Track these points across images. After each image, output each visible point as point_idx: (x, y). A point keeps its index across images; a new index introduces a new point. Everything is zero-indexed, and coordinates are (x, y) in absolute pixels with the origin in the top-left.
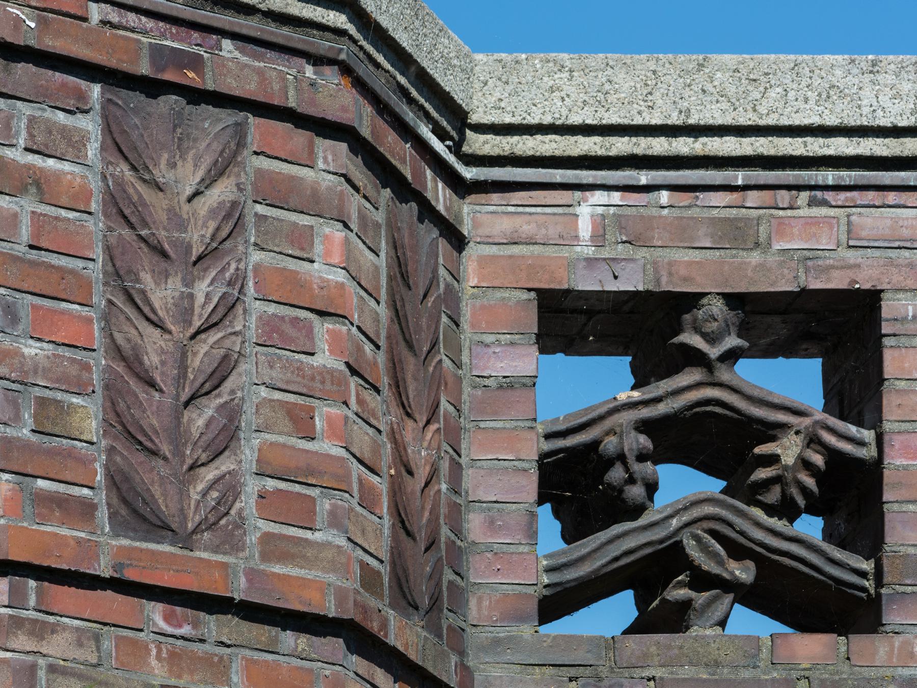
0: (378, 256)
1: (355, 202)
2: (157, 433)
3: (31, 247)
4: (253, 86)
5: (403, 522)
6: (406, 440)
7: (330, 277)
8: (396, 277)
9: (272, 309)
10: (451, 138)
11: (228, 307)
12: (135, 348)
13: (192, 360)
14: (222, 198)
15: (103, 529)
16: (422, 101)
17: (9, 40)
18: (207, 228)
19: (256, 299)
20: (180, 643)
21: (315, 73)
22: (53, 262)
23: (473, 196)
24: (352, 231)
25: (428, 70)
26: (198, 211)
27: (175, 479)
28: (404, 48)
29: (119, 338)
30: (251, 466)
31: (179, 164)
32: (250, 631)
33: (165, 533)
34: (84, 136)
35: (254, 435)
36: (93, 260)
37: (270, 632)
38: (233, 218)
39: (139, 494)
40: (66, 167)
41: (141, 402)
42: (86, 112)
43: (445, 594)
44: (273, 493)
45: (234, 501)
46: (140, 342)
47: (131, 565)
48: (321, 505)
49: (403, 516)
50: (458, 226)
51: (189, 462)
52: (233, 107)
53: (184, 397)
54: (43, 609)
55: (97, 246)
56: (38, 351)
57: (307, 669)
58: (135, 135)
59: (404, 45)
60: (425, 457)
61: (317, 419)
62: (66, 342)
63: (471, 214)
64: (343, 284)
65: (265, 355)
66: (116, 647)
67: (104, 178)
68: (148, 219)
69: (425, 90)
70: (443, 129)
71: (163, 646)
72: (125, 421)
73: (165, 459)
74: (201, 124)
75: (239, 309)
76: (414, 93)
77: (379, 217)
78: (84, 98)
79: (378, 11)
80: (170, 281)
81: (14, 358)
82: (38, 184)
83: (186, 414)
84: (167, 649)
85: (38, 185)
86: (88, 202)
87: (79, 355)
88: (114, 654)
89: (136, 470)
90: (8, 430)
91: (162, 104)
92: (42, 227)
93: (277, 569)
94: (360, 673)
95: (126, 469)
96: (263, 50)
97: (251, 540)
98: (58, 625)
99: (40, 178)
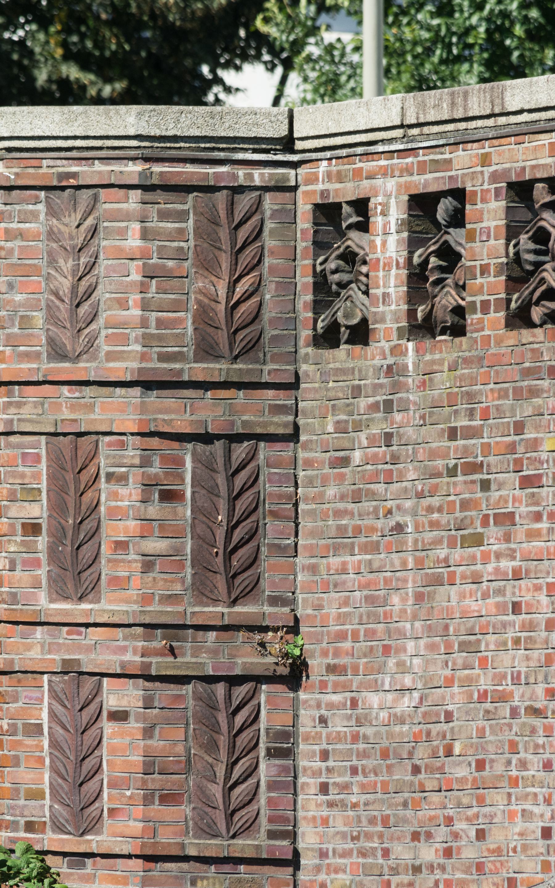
40: (33, 225)
82: (21, 234)
83: (79, 310)
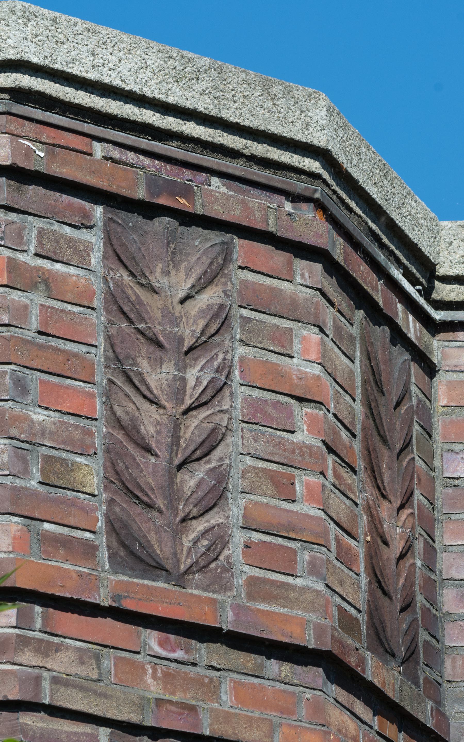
0: (353, 363)
1: (329, 315)
2: (152, 489)
3: (40, 333)
4: (237, 213)
5: (379, 582)
6: (381, 515)
7: (308, 370)
8: (369, 382)
9: (256, 393)
10: (421, 284)
11: (215, 391)
12: (133, 419)
13: (185, 433)
14: (211, 301)
15: (103, 566)
16: (393, 247)
17: (21, 165)
18: (197, 324)
19: (241, 385)
20: (173, 665)
21: (293, 208)
22: (59, 346)
23: (442, 334)
24: (328, 336)
25: (397, 222)
26: (189, 312)
27: (169, 528)
28: (374, 199)
29: (119, 411)
30: (238, 520)
31: (173, 272)
32: (238, 658)
33: (159, 572)
34: (88, 246)
35: (240, 495)
36: (96, 346)
37: (256, 659)
38: (220, 321)
39: (136, 539)
40: (72, 270)
41: (138, 463)
42: (91, 227)
43: (421, 651)
44: (258, 544)
45: (223, 549)
46: (137, 414)
47: (128, 596)
48: (302, 556)
49: (380, 577)
50: (428, 354)
51: (181, 515)
52: (220, 229)
53: (177, 461)
54: (48, 630)
55: (99, 335)
56: (45, 418)
57: (290, 692)
58: (133, 248)
59: (375, 196)
60: (400, 534)
61: (297, 485)
62: (71, 411)
63: (439, 348)
64: (319, 376)
65: (250, 431)
66: (115, 665)
67: (106, 281)
68: (145, 315)
69: (395, 239)
70: (413, 275)
71: (158, 667)
72: (124, 479)
73: (160, 511)
74: (191, 242)
75: (226, 392)
76: (385, 240)
77: (355, 331)
78: (88, 216)
79: (349, 164)
80: (164, 366)
81: (23, 423)
83: (179, 476)
84: (162, 670)
85: (47, 283)
86: (91, 299)
87: (83, 423)
88: (113, 672)
89: (134, 520)
90: (17, 481)
91: (157, 224)
92: (51, 317)
93: (262, 606)
94: (340, 700)
95: (124, 517)
96: (247, 187)
97: (238, 582)
98: (62, 645)
99: (48, 278)
